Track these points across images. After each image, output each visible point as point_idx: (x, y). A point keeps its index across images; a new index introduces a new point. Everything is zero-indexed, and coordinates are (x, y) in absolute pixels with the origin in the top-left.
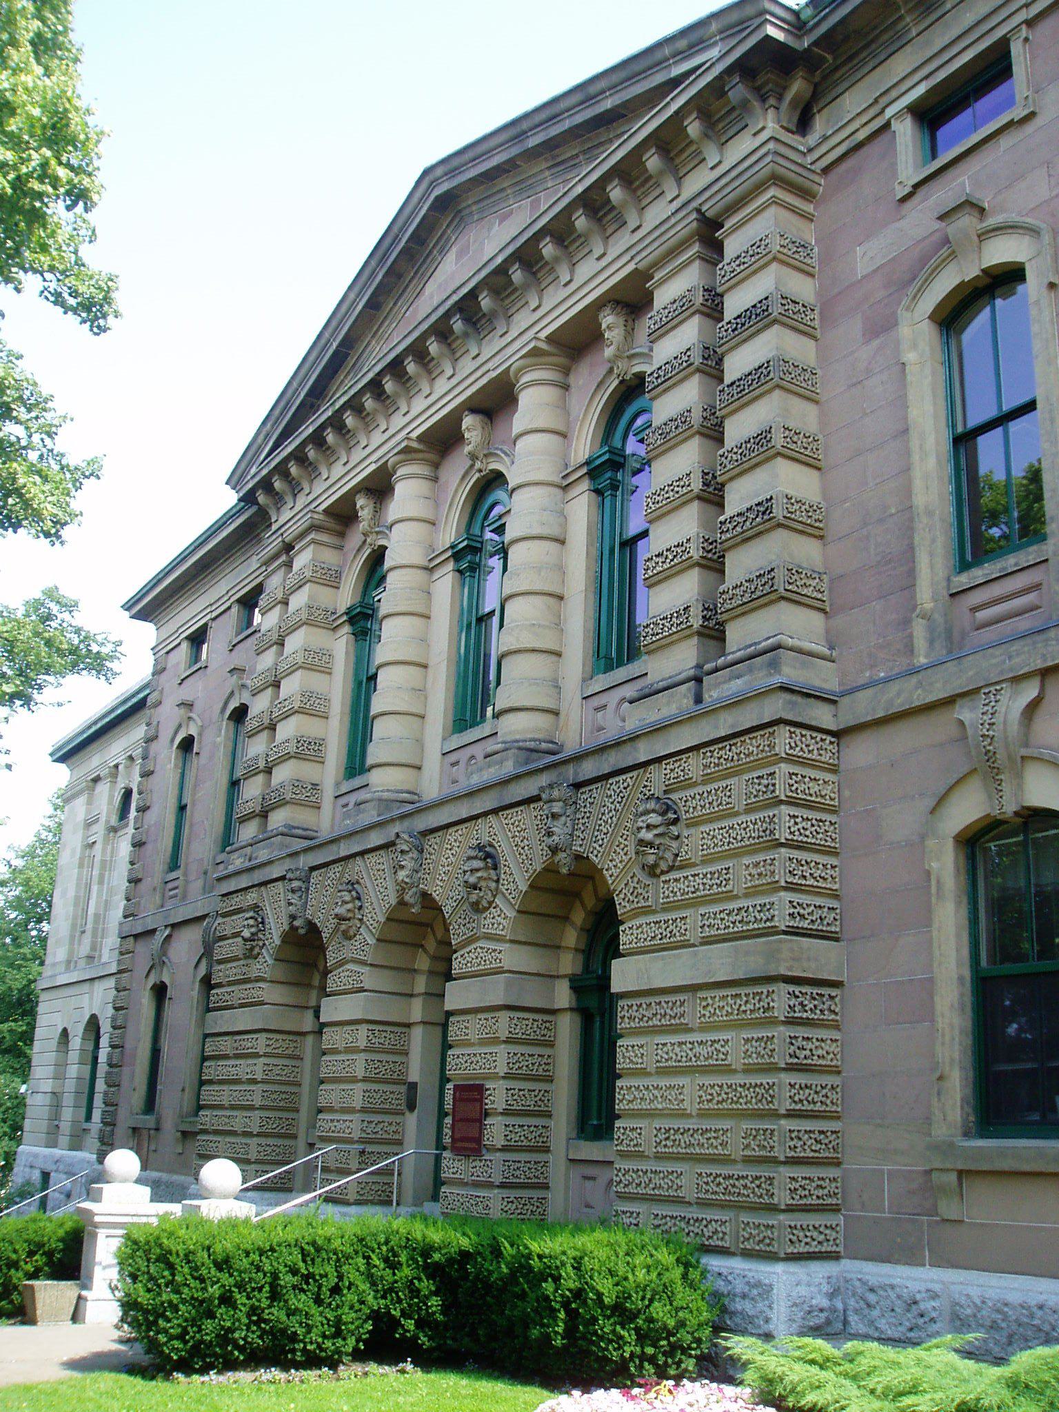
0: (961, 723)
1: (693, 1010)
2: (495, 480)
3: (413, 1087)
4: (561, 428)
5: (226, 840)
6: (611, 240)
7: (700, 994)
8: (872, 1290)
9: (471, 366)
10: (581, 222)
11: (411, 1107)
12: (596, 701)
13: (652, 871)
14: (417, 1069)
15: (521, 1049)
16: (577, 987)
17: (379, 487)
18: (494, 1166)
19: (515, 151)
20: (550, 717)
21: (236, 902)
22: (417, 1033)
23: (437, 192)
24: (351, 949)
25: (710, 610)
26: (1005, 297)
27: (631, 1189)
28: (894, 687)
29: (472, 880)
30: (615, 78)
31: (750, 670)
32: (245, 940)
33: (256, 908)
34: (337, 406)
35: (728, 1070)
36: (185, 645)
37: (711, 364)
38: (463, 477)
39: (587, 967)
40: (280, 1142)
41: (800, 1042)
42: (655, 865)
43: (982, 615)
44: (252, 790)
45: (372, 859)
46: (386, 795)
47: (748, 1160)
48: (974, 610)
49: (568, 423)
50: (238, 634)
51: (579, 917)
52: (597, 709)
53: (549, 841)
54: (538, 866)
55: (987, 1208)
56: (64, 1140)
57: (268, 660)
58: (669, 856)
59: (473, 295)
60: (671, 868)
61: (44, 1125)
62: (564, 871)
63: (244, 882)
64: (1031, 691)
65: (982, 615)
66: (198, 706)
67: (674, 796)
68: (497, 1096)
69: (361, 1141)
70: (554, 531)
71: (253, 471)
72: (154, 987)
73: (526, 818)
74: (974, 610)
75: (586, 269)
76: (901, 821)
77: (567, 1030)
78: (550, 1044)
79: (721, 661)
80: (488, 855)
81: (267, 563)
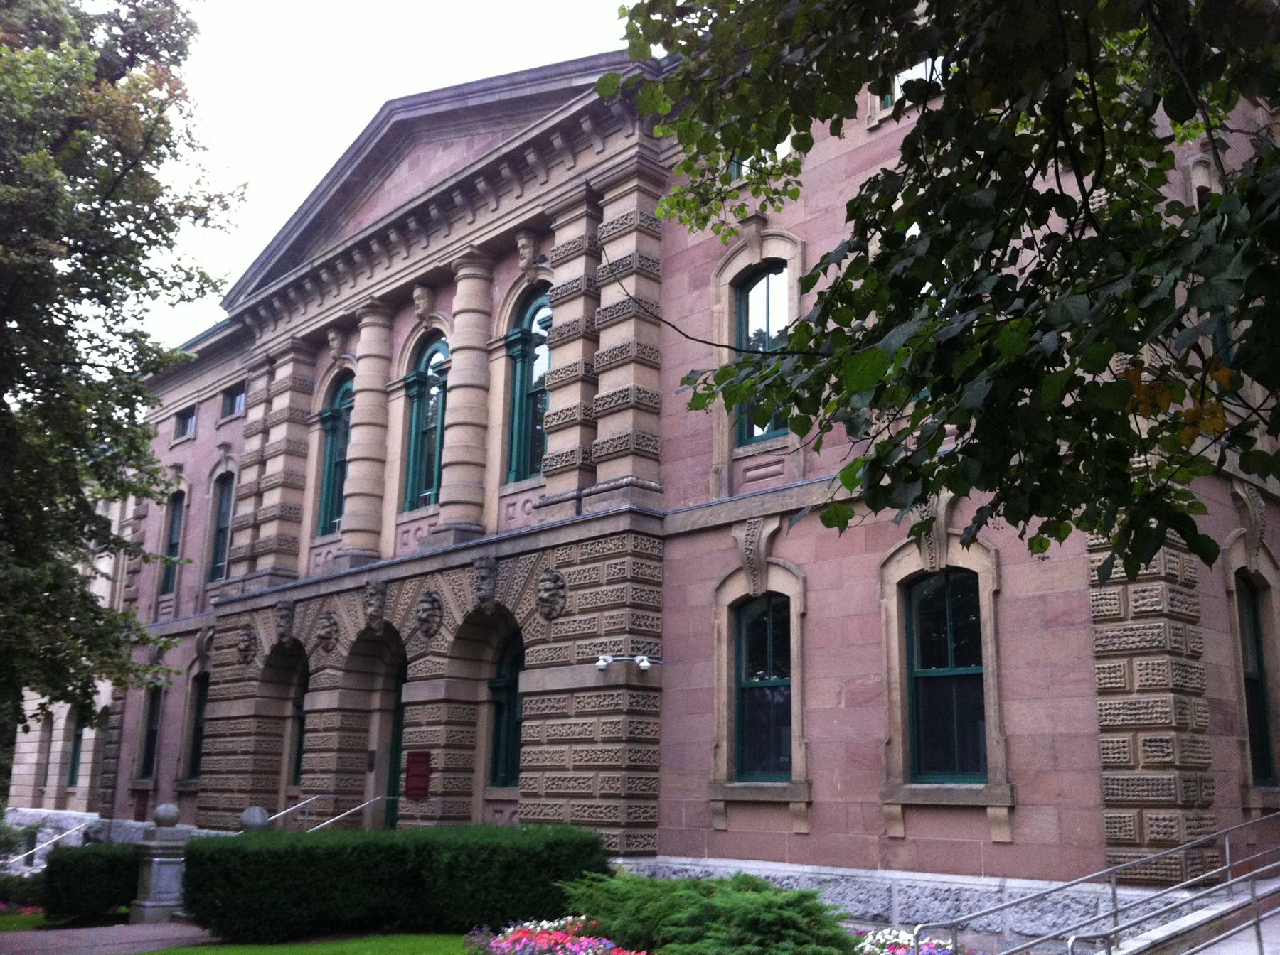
0: (735, 539)
1: (573, 706)
2: (438, 334)
3: (372, 754)
4: (487, 309)
5: (214, 572)
6: (526, 186)
7: (576, 695)
8: (674, 873)
9: (423, 254)
10: (506, 172)
11: (371, 767)
12: (509, 500)
13: (548, 617)
14: (375, 738)
15: (455, 728)
16: (493, 689)
17: (348, 327)
18: (433, 806)
19: (457, 105)
20: (477, 509)
21: (232, 622)
22: (376, 719)
23: (396, 118)
24: (331, 659)
25: (588, 366)
26: (776, 273)
27: (529, 816)
28: (697, 514)
29: (424, 616)
30: (533, 76)
31: (612, 498)
32: (241, 651)
33: (247, 627)
34: (316, 264)
35: (591, 741)
36: (173, 420)
37: (591, 291)
38: (414, 330)
39: (499, 676)
40: (265, 796)
41: (635, 725)
42: (550, 613)
43: (750, 474)
44: (243, 540)
45: (346, 597)
46: (356, 552)
47: (604, 796)
48: (747, 470)
49: (491, 307)
50: (223, 417)
51: (495, 641)
52: (509, 505)
53: (479, 594)
54: (470, 608)
55: (741, 822)
56: (50, 800)
57: (255, 443)
58: (558, 607)
59: (425, 205)
60: (559, 616)
61: (29, 791)
62: (488, 613)
63: (238, 608)
64: (773, 525)
65: (750, 474)
66: (188, 469)
67: (563, 571)
68: (439, 758)
69: (335, 792)
70: (481, 381)
71: (242, 299)
72: (196, 678)
73: (466, 578)
74: (747, 470)
75: (508, 203)
76: (700, 593)
77: (484, 715)
78: (474, 724)
79: (593, 489)
80: (435, 603)
81: (254, 369)
